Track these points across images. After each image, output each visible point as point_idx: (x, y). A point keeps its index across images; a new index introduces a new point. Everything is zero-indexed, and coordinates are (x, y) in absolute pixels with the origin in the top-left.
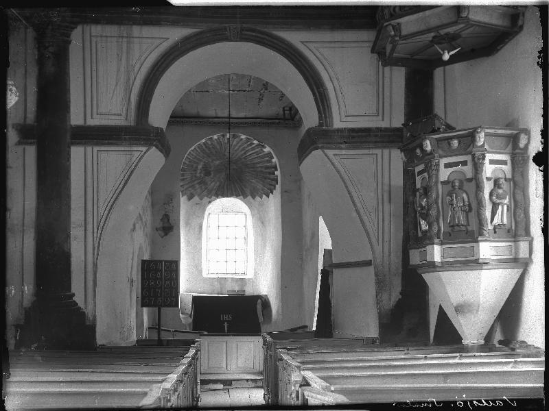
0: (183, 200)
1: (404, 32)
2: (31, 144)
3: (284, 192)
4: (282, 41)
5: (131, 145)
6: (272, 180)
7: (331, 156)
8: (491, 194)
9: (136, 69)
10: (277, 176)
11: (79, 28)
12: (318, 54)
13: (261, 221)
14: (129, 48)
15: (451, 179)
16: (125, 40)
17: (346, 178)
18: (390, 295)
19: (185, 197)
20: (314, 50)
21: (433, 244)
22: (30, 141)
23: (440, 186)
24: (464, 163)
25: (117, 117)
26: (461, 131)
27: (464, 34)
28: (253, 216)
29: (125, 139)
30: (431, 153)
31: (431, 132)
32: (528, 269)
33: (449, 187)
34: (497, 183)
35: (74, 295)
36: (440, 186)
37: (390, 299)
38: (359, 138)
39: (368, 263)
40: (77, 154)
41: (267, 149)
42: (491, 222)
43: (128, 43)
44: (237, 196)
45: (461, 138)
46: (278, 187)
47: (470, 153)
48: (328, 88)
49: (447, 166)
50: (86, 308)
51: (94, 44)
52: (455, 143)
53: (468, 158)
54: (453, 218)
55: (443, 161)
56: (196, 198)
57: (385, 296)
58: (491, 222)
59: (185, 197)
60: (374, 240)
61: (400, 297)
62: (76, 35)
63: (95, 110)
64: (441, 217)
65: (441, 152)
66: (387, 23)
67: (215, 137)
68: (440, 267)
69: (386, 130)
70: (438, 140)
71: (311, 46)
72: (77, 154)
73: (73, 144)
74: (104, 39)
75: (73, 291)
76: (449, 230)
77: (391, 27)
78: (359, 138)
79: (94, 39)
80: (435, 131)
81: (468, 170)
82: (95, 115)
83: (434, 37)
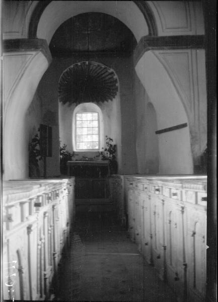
0: (60, 104)
3: (122, 96)
13: (108, 115)
19: (61, 102)
25: (17, 34)
28: (103, 113)
32: (128, 213)
37: (200, 149)
39: (184, 125)
41: (111, 70)
44: (93, 101)
46: (118, 93)
56: (67, 103)
57: (197, 147)
59: (61, 102)
67: (79, 64)
69: (193, 36)
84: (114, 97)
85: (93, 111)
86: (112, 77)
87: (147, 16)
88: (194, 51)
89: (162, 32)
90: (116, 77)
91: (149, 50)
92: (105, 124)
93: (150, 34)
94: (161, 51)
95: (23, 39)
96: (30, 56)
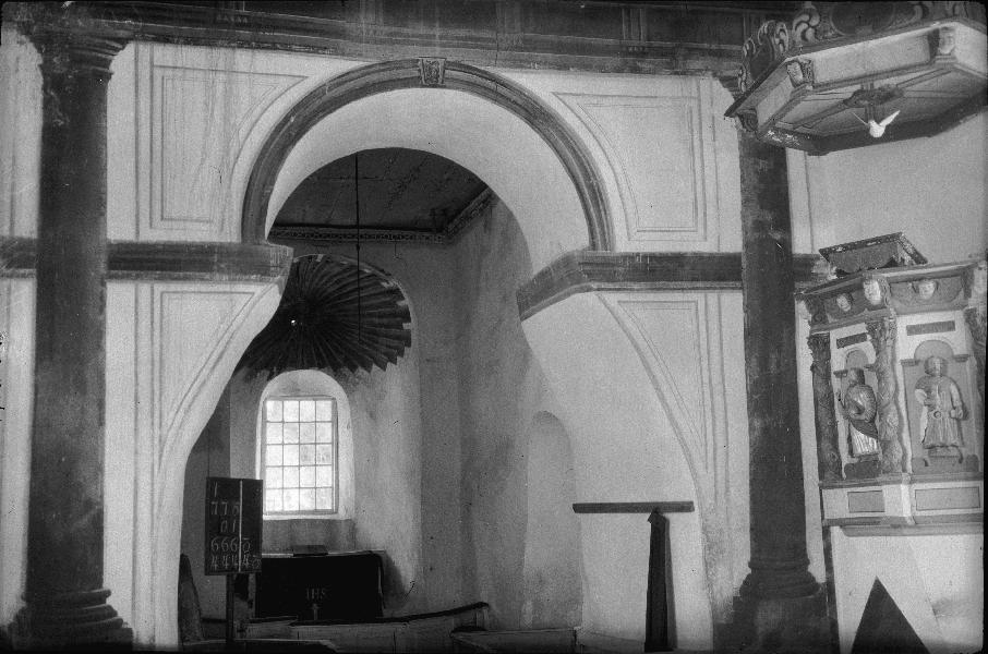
1: (821, 77)
4: (520, 92)
5: (232, 281)
6: (398, 338)
7: (620, 311)
9: (243, 133)
10: (409, 332)
11: (130, 48)
14: (228, 93)
15: (923, 356)
16: (222, 76)
20: (576, 108)
21: (900, 482)
22: (22, 271)
23: (899, 368)
24: (950, 326)
26: (935, 266)
27: (911, 92)
28: (352, 402)
29: (220, 270)
30: (882, 306)
31: (886, 266)
33: (919, 372)
35: (108, 593)
37: (731, 578)
38: (662, 271)
40: (123, 302)
43: (228, 82)
44: (321, 367)
45: (939, 278)
48: (606, 179)
49: (912, 330)
51: (158, 83)
52: (928, 288)
54: (932, 430)
55: (903, 323)
57: (721, 572)
60: (699, 465)
61: (750, 571)
62: (123, 63)
64: (906, 428)
65: (898, 305)
66: (792, 59)
68: (910, 527)
70: (892, 282)
72: (123, 302)
73: (111, 277)
74: (179, 73)
76: (924, 454)
77: (798, 67)
78: (662, 271)
79: (158, 73)
80: (892, 264)
83: (855, 94)
84: (394, 362)
85: (316, 396)
86: (392, 304)
87: (586, 190)
88: (712, 297)
89: (628, 240)
90: (406, 302)
91: (589, 289)
92: (356, 438)
93: (594, 246)
94: (622, 296)
95: (221, 246)
96: (245, 298)
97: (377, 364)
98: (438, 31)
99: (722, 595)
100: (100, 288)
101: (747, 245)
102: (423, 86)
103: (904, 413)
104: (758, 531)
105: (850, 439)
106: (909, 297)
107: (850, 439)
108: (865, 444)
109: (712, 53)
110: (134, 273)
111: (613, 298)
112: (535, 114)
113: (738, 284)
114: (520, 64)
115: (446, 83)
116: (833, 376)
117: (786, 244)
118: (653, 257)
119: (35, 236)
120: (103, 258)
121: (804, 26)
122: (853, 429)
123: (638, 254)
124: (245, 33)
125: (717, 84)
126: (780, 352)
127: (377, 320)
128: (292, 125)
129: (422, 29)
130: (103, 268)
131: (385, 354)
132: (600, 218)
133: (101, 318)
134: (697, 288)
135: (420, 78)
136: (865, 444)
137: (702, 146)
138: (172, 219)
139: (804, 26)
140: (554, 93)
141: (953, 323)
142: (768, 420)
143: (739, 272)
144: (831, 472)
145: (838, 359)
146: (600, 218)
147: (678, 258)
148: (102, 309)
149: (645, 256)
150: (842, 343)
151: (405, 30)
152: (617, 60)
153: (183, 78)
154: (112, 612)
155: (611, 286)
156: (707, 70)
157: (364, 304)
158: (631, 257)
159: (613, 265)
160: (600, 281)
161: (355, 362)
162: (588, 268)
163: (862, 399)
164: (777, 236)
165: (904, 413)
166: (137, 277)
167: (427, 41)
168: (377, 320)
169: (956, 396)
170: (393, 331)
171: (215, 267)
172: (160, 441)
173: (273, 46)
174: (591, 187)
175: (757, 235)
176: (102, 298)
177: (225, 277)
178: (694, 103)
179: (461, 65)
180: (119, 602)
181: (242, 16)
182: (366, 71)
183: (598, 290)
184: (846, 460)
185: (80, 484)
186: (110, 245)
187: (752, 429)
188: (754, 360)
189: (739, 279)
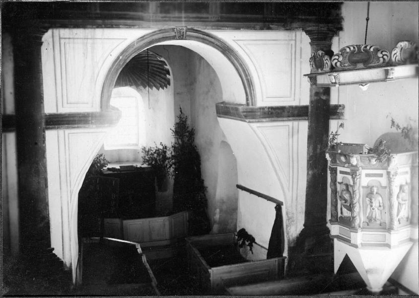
2: (10, 131)
7: (256, 129)
8: (398, 197)
9: (100, 65)
11: (50, 32)
12: (247, 51)
17: (265, 143)
18: (296, 227)
20: (242, 46)
23: (361, 189)
24: (381, 175)
34: (401, 187)
35: (53, 249)
36: (361, 189)
37: (296, 230)
38: (276, 113)
42: (397, 216)
47: (386, 169)
49: (368, 175)
50: (63, 258)
53: (383, 172)
54: (371, 212)
58: (397, 216)
60: (286, 190)
61: (304, 227)
63: (65, 101)
71: (240, 43)
73: (48, 129)
75: (52, 246)
77: (333, 77)
78: (276, 113)
81: (383, 181)
82: (65, 104)
88: (296, 123)
89: (262, 101)
90: (168, 67)
93: (248, 104)
97: (155, 86)
98: (183, 15)
99: (292, 236)
100: (43, 133)
101: (311, 102)
102: (177, 39)
103: (362, 206)
104: (308, 213)
105: (341, 209)
106: (367, 162)
107: (341, 209)
108: (346, 213)
109: (302, 20)
110: (56, 126)
111: (255, 125)
112: (226, 50)
113: (307, 118)
114: (219, 28)
115: (187, 38)
116: (337, 183)
117: (328, 100)
118: (272, 108)
119: (14, 114)
120: (44, 121)
121: (336, 61)
122: (343, 207)
123: (266, 107)
124: (99, 21)
125: (304, 33)
126: (322, 144)
127: (155, 69)
128: (121, 60)
129: (177, 15)
130: (43, 125)
131: (160, 84)
132: (251, 93)
133: (44, 145)
134: (290, 120)
135: (176, 36)
136: (346, 213)
137: (295, 61)
138: (70, 103)
139: (336, 61)
140: (233, 40)
141: (382, 174)
142: (316, 170)
143: (307, 113)
144: (336, 219)
145: (340, 177)
146: (251, 93)
147: (282, 109)
148: (44, 142)
149: (269, 108)
150: (341, 172)
151: (168, 15)
152: (261, 24)
153: (74, 43)
154: (55, 255)
155: (254, 120)
156: (300, 28)
157: (150, 62)
158: (263, 108)
159: (255, 112)
160: (249, 119)
161: (146, 84)
162: (245, 114)
163: (347, 196)
164: (324, 98)
165: (362, 206)
166: (58, 128)
167: (179, 19)
168: (155, 69)
169: (381, 201)
170: (162, 75)
171: (90, 122)
172: (70, 192)
173: (111, 26)
174: (248, 80)
175: (316, 98)
176: (44, 137)
177: (94, 126)
178: (293, 42)
179: (194, 30)
180: (57, 252)
181: (98, 14)
182: (154, 33)
183: (249, 122)
184: (339, 215)
185: (39, 211)
186: (46, 115)
187: (308, 174)
188: (311, 147)
189: (307, 116)
